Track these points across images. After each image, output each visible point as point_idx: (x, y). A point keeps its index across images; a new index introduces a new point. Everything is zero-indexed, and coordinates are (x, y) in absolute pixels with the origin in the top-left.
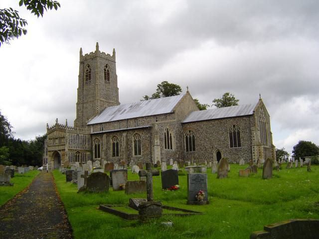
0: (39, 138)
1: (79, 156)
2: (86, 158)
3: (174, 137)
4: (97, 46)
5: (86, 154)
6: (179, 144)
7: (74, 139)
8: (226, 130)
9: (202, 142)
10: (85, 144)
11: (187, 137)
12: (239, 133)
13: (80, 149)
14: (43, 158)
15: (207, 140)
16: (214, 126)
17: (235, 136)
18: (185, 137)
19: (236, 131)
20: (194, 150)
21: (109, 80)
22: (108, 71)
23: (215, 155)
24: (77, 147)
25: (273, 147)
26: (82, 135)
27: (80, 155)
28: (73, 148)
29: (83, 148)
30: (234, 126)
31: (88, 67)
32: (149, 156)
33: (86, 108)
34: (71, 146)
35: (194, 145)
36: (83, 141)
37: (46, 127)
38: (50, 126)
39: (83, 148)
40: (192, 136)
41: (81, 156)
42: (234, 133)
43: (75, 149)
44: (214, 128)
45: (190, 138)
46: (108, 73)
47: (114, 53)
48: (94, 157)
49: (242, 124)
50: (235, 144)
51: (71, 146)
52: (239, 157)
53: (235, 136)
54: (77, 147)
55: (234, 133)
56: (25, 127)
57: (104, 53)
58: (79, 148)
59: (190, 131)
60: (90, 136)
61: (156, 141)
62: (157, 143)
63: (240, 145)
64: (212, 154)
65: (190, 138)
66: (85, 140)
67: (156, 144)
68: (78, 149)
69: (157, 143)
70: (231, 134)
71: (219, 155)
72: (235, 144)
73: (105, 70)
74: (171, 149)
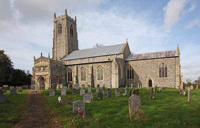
1: (58, 79)
10: (62, 72)
11: (128, 70)
12: (166, 68)
13: (58, 75)
15: (143, 72)
16: (148, 63)
17: (130, 73)
19: (164, 67)
20: (133, 78)
21: (73, 34)
22: (72, 29)
26: (60, 66)
27: (58, 79)
28: (54, 74)
30: (163, 64)
31: (60, 25)
32: (109, 81)
33: (59, 51)
37: (33, 59)
38: (36, 58)
42: (163, 68)
45: (130, 71)
46: (72, 31)
50: (163, 75)
53: (130, 73)
55: (163, 68)
56: (22, 62)
63: (166, 76)
65: (130, 71)
70: (160, 68)
72: (163, 75)
73: (71, 28)
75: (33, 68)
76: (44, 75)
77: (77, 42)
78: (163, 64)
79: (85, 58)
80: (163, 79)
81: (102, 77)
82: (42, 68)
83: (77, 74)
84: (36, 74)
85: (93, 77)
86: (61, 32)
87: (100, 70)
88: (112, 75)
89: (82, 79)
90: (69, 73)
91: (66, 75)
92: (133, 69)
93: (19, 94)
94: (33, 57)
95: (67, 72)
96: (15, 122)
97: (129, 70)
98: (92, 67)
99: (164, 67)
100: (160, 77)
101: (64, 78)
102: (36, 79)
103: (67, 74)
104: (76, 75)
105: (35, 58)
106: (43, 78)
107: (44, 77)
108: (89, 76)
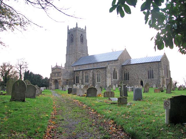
3: (118, 73)
12: (152, 71)
15: (136, 74)
17: (126, 75)
19: (151, 70)
20: (129, 80)
21: (83, 42)
22: (82, 37)
27: (68, 82)
28: (65, 78)
30: (150, 67)
41: (69, 82)
42: (150, 71)
45: (126, 74)
48: (96, 82)
53: (126, 75)
59: (126, 70)
60: (73, 72)
62: (109, 75)
64: (138, 82)
66: (71, 74)
69: (109, 75)
73: (81, 37)
74: (117, 79)
75: (51, 74)
76: (58, 79)
77: (87, 48)
78: (150, 67)
79: (91, 64)
80: (151, 80)
81: (100, 80)
82: (57, 74)
83: (82, 77)
84: (53, 78)
85: (93, 79)
86: (73, 42)
87: (98, 74)
88: (107, 78)
89: (86, 81)
90: (76, 77)
91: (74, 78)
93: (29, 80)
94: (152, 37)
95: (75, 76)
96: (43, 8)
98: (93, 72)
99: (151, 70)
100: (149, 78)
101: (73, 81)
102: (52, 82)
103: (75, 77)
104: (81, 78)
105: (68, 28)
106: (57, 81)
107: (58, 80)
108: (91, 79)
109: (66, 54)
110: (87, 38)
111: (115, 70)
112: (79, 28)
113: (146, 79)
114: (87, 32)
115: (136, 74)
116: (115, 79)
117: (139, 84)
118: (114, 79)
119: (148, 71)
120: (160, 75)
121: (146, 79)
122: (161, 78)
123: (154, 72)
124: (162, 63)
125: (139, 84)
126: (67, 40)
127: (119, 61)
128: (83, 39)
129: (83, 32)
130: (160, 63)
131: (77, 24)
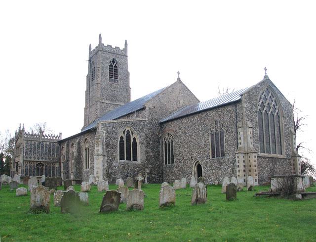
0: (296, 127)
2: (53, 172)
3: (142, 143)
4: (100, 38)
5: (53, 168)
6: (151, 154)
7: (35, 148)
8: (206, 130)
9: (181, 150)
12: (222, 133)
13: (44, 160)
14: (11, 170)
15: (186, 146)
16: (193, 124)
18: (164, 142)
20: (173, 162)
21: (116, 77)
22: (115, 66)
23: (194, 169)
24: (38, 158)
25: (295, 156)
26: (48, 143)
27: (44, 168)
28: (33, 160)
29: (50, 159)
34: (29, 156)
35: (173, 156)
36: (50, 151)
39: (50, 159)
40: (170, 142)
43: (36, 160)
44: (194, 127)
47: (126, 44)
49: (227, 116)
51: (29, 156)
52: (222, 174)
54: (38, 158)
57: (111, 46)
58: (42, 158)
59: (169, 134)
61: (96, 149)
62: (98, 150)
63: (223, 155)
64: (191, 167)
67: (96, 153)
68: (40, 160)
69: (98, 150)
71: (199, 168)
73: (111, 65)
74: (135, 159)
80: (219, 162)
92: (172, 141)
97: (167, 142)
109: (84, 106)
110: (131, 68)
111: (128, 137)
112: (106, 45)
113: (208, 160)
114: (129, 54)
115: (186, 146)
116: (129, 158)
117: (193, 173)
118: (122, 158)
119: (212, 135)
120: (239, 146)
121: (208, 160)
122: (241, 156)
123: (226, 136)
124: (245, 105)
125: (193, 173)
126: (87, 77)
127: (146, 112)
128: (116, 71)
129: (117, 54)
130: (239, 106)
131: (100, 38)
